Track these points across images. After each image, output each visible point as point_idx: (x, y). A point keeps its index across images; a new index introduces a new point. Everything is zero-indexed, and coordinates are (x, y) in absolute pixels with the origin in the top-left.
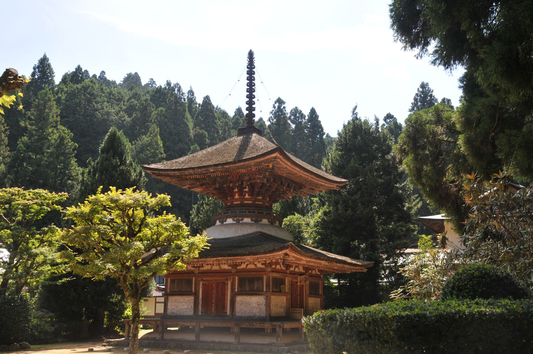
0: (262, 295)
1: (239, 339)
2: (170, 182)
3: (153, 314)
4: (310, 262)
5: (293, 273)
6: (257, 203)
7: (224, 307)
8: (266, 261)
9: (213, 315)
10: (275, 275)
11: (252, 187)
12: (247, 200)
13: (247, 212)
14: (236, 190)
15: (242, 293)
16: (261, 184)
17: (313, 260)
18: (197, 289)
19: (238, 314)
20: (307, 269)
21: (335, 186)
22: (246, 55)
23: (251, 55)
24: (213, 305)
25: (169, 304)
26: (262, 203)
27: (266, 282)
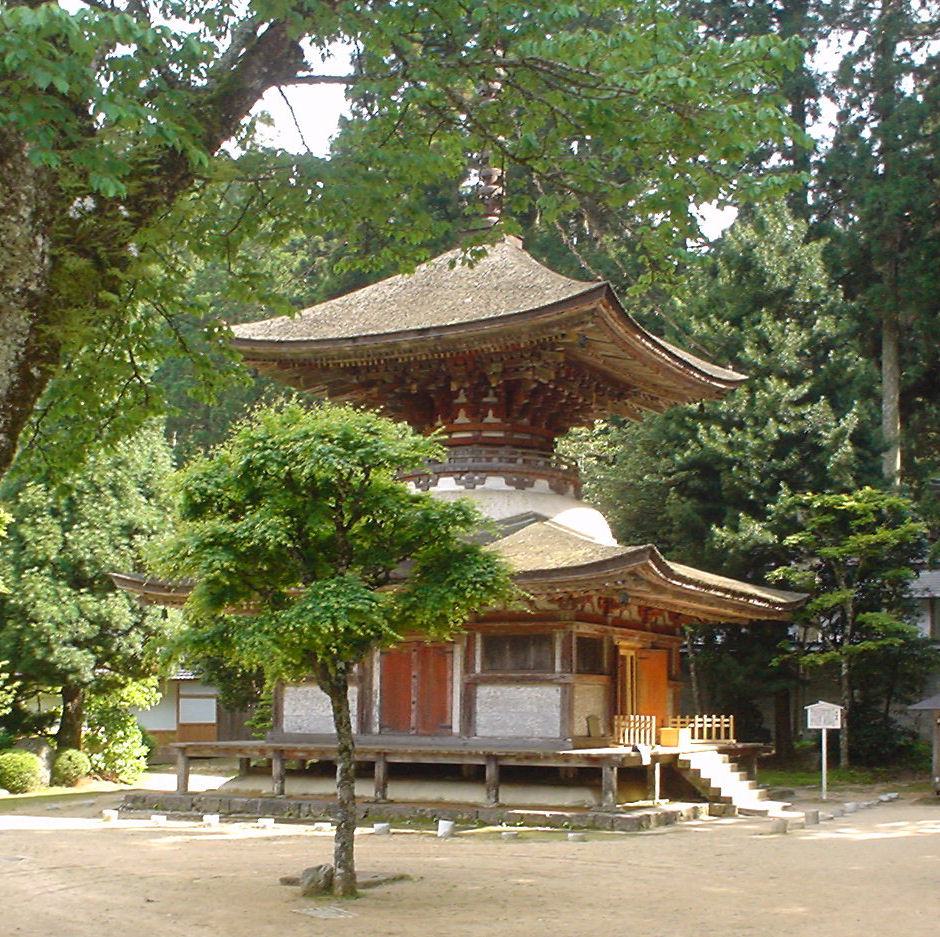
0: (550, 682)
1: (497, 795)
6: (485, 434)
7: (443, 713)
14: (462, 399)
16: (534, 386)
24: (413, 707)
25: (286, 705)
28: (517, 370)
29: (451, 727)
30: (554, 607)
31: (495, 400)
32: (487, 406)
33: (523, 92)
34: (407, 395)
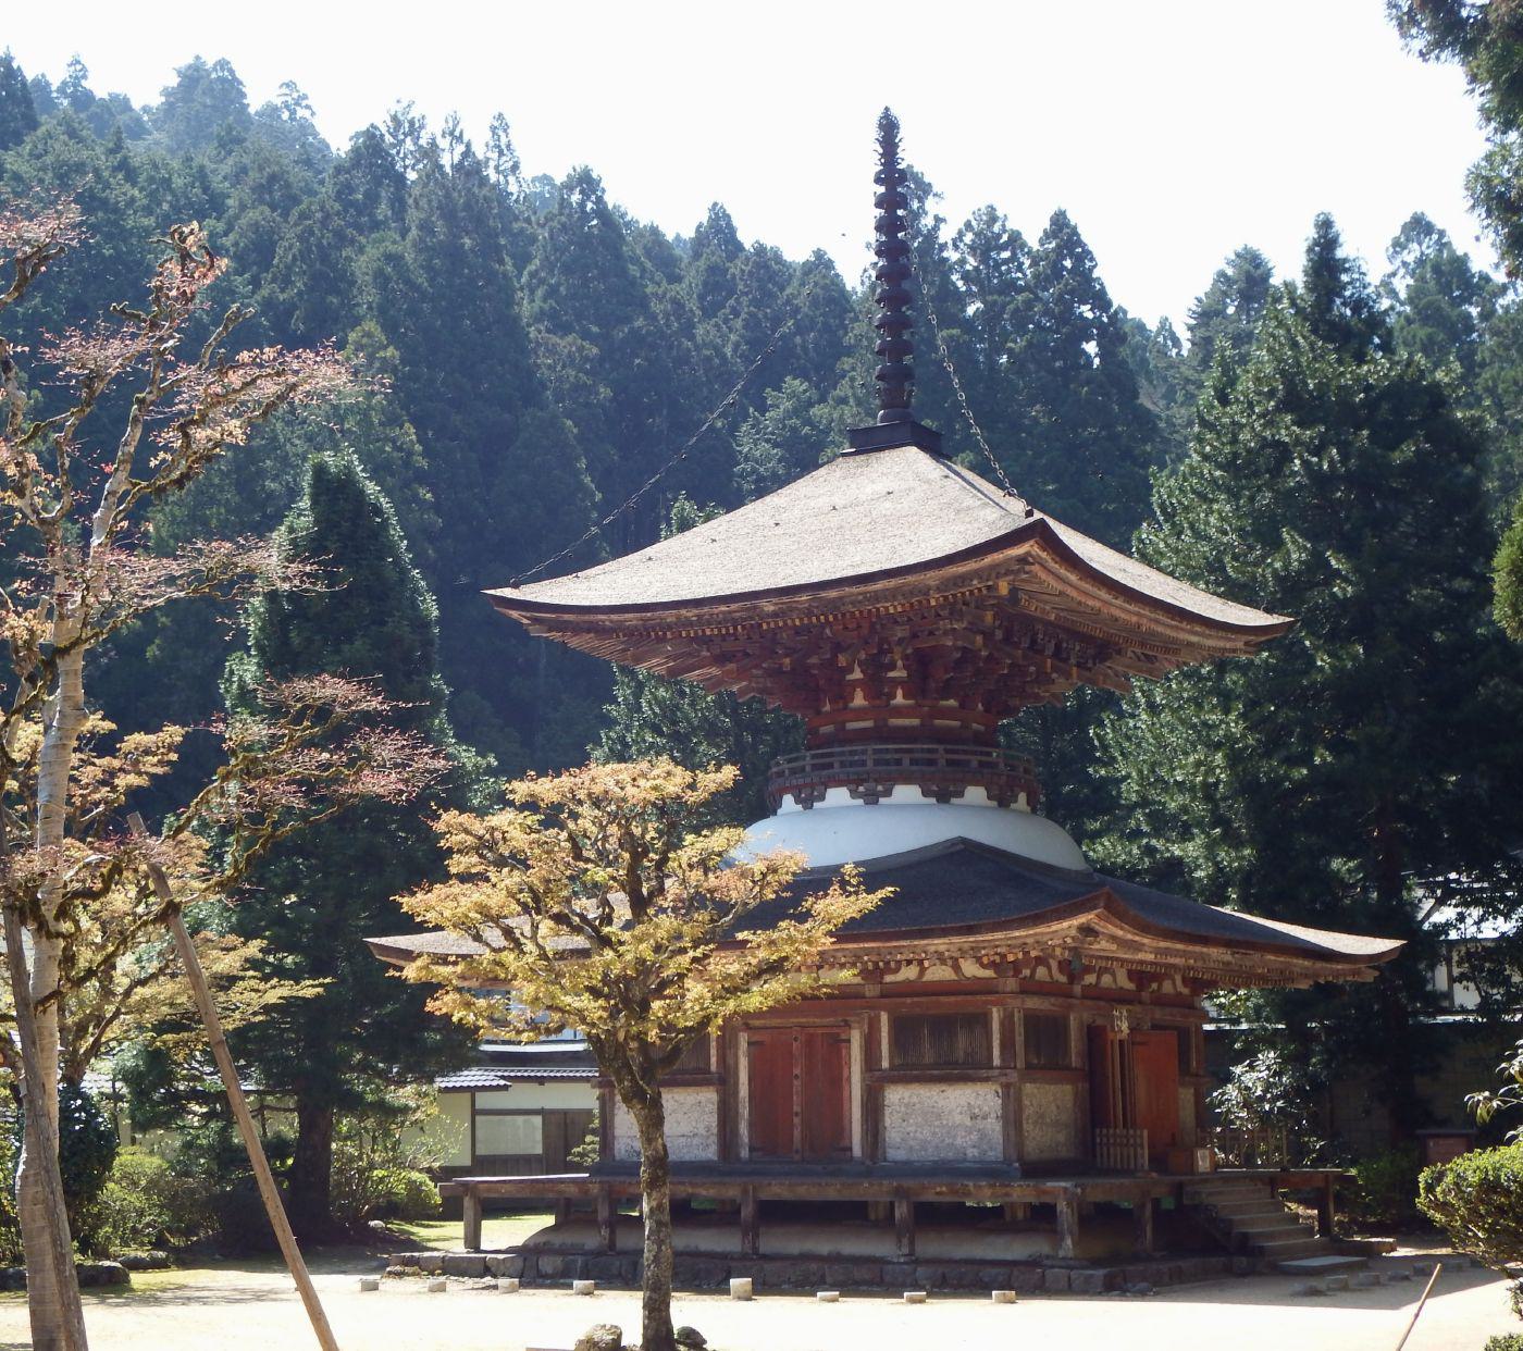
0: (987, 1080)
1: (912, 1243)
2: (594, 649)
3: (467, 1162)
4: (1166, 952)
5: (1095, 995)
6: (937, 722)
8: (1003, 956)
9: (797, 1157)
10: (1033, 1003)
11: (922, 664)
12: (899, 712)
13: (906, 762)
14: (857, 674)
15: (910, 1071)
17: (1180, 946)
18: (730, 1061)
19: (895, 1154)
20: (1141, 976)
21: (1240, 645)
22: (873, 133)
23: (889, 129)
24: (796, 1120)
26: (956, 723)
27: (1003, 1034)
28: (931, 633)
29: (851, 1149)
30: (989, 973)
31: (904, 674)
32: (895, 682)
33: (488, 945)
34: (777, 673)
